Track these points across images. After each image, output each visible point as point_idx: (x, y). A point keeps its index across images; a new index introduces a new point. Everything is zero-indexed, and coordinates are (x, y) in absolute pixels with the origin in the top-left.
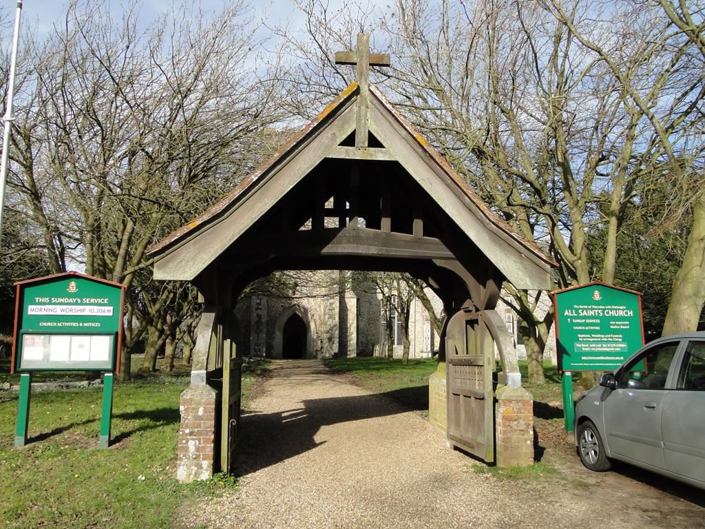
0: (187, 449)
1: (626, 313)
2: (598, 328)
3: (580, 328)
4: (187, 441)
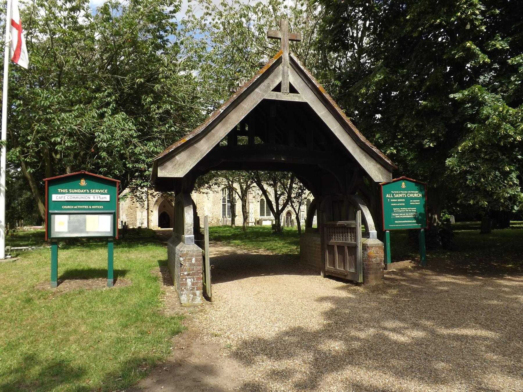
0: (186, 284)
1: (419, 195)
2: (404, 204)
3: (394, 204)
4: (186, 279)
